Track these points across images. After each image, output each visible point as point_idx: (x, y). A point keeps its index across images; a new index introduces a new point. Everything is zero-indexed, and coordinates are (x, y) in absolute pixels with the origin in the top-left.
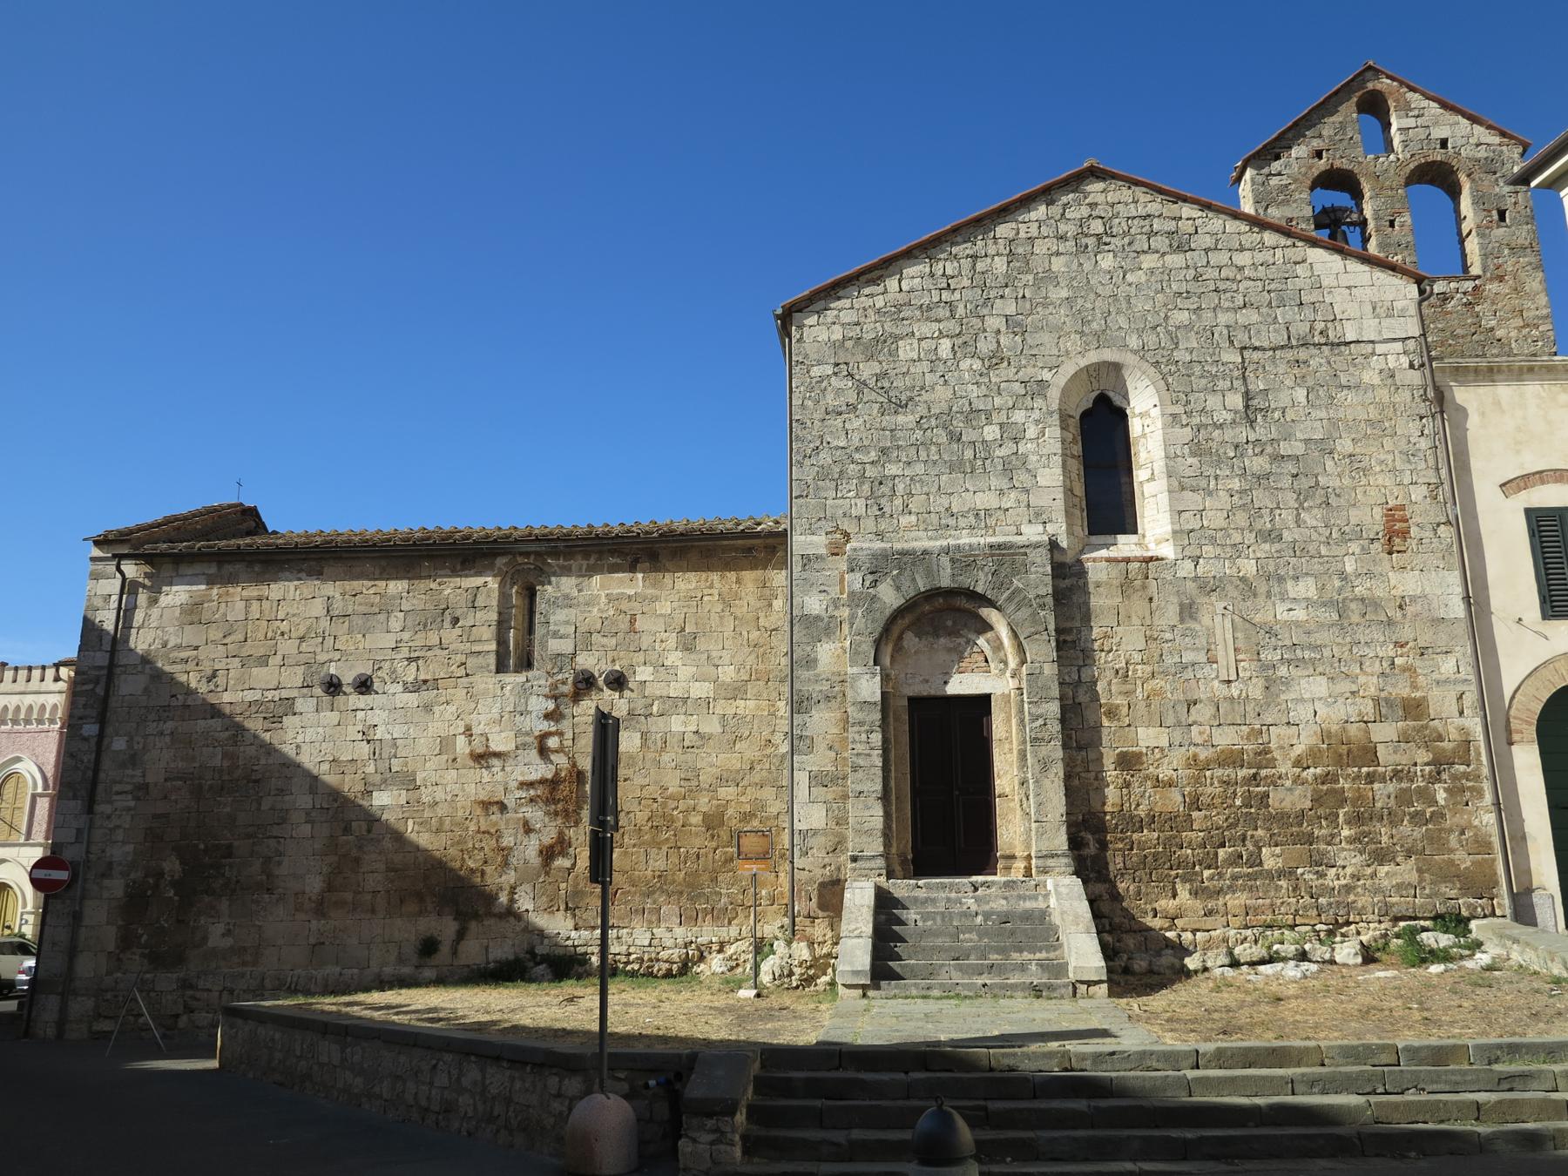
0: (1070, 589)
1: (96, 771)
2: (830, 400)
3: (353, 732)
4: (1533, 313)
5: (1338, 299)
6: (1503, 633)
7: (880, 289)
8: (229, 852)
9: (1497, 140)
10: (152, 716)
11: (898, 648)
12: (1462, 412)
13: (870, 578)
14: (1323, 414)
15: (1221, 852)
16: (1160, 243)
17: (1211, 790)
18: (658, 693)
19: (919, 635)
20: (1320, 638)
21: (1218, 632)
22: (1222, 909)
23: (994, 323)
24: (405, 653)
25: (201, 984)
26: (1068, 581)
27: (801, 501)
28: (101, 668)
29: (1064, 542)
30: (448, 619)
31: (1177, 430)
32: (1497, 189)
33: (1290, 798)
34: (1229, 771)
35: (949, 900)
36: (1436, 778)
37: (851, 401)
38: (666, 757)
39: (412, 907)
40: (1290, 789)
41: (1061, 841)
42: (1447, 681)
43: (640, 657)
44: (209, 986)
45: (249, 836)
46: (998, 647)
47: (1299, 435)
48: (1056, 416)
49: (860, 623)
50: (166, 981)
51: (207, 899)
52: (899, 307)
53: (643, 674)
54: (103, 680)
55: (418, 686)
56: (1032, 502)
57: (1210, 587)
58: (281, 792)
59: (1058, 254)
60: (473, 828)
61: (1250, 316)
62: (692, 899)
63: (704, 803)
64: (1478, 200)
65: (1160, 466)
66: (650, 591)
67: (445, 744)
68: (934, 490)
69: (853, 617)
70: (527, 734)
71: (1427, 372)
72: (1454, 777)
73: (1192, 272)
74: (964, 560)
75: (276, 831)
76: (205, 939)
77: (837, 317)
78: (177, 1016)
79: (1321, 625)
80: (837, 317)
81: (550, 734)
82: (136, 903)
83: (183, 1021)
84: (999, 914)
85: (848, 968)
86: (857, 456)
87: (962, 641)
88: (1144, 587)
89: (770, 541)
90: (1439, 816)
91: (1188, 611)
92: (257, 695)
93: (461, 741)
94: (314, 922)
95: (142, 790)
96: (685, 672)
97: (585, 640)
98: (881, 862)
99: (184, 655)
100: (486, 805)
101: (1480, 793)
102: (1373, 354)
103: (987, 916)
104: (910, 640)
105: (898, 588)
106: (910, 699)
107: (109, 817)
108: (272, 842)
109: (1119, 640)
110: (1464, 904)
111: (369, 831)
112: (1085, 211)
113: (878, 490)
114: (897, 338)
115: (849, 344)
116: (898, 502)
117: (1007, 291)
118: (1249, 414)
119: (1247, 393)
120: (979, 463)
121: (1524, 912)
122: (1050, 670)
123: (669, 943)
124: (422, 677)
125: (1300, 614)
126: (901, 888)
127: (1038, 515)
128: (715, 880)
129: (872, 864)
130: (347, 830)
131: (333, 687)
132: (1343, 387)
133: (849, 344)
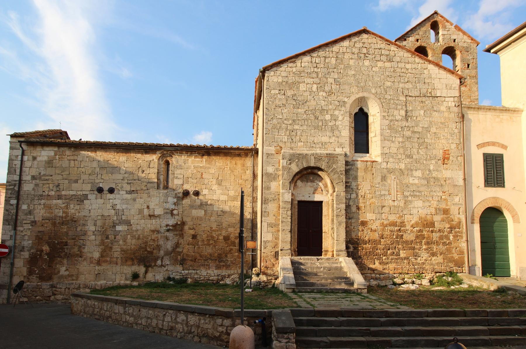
0: (349, 169)
1: (17, 215)
2: (277, 102)
3: (109, 206)
4: (473, 98)
5: (436, 82)
6: (474, 190)
7: (295, 65)
8: (66, 244)
9: (470, 41)
10: (36, 198)
11: (295, 185)
12: (470, 120)
13: (289, 162)
14: (428, 119)
15: (389, 251)
16: (384, 58)
17: (387, 233)
18: (210, 198)
19: (302, 181)
20: (421, 189)
21: (392, 185)
22: (388, 268)
23: (331, 80)
24: (126, 181)
25: (58, 286)
26: (349, 165)
27: (267, 135)
28: (16, 181)
29: (348, 153)
30: (140, 171)
31: (385, 121)
32: (468, 57)
33: (409, 237)
34: (392, 227)
35: (311, 263)
36: (450, 232)
37: (284, 103)
38: (212, 218)
39: (130, 263)
40: (409, 234)
41: (344, 247)
42: (456, 204)
43: (204, 186)
44: (61, 287)
45: (73, 239)
46: (326, 186)
47: (421, 125)
48: (348, 113)
49: (285, 176)
50: (45, 285)
51: (59, 259)
52: (300, 72)
53: (205, 192)
54: (18, 185)
55: (131, 192)
56: (341, 141)
57: (391, 171)
58: (84, 225)
59: (352, 59)
60: (150, 238)
61: (409, 86)
62: (220, 262)
63: (224, 233)
64: (463, 60)
65: (378, 132)
66: (208, 165)
67: (141, 211)
68: (309, 135)
69: (283, 174)
70: (168, 209)
71: (460, 108)
72: (456, 232)
73: (393, 69)
74: (319, 158)
75: (82, 238)
76: (59, 272)
77: (280, 73)
78: (50, 296)
79: (422, 185)
80: (280, 73)
81: (175, 209)
82: (33, 261)
83: (52, 298)
84: (328, 268)
85: (288, 283)
86: (285, 122)
87: (315, 184)
88: (371, 170)
89: (246, 152)
90: (450, 243)
91: (384, 178)
92: (74, 193)
93: (146, 210)
94: (97, 267)
95: (34, 223)
96: (218, 192)
97: (186, 180)
98: (289, 251)
99: (47, 178)
100: (153, 231)
101: (462, 237)
102: (445, 101)
103: (324, 268)
104: (299, 183)
105: (297, 166)
106: (299, 201)
107: (22, 231)
108: (81, 241)
109: (364, 186)
110: (455, 269)
111: (115, 238)
112: (361, 45)
113: (292, 133)
114: (299, 83)
115: (284, 83)
116: (298, 138)
117: (335, 70)
118: (406, 117)
119: (407, 110)
120: (324, 127)
121: (471, 271)
122: (343, 194)
123: (213, 275)
124: (132, 189)
125: (416, 181)
126: (302, 259)
127: (341, 145)
128: (226, 256)
129: (287, 252)
130: (107, 238)
131: (100, 190)
132: (435, 111)
133: (284, 83)
